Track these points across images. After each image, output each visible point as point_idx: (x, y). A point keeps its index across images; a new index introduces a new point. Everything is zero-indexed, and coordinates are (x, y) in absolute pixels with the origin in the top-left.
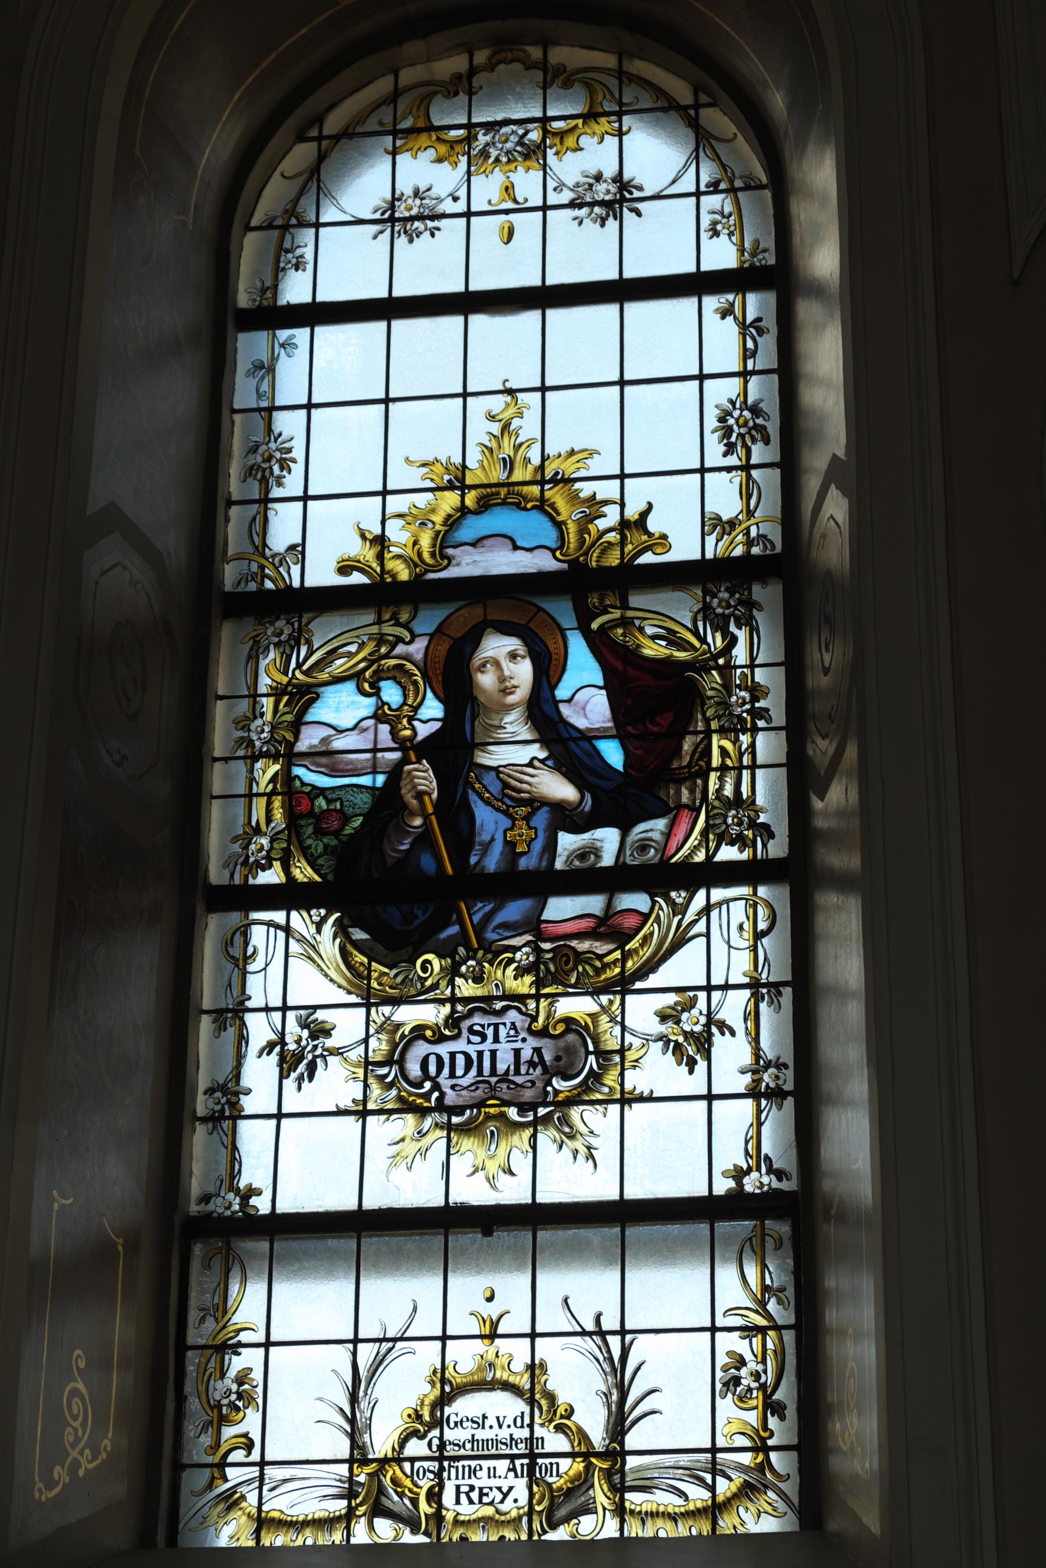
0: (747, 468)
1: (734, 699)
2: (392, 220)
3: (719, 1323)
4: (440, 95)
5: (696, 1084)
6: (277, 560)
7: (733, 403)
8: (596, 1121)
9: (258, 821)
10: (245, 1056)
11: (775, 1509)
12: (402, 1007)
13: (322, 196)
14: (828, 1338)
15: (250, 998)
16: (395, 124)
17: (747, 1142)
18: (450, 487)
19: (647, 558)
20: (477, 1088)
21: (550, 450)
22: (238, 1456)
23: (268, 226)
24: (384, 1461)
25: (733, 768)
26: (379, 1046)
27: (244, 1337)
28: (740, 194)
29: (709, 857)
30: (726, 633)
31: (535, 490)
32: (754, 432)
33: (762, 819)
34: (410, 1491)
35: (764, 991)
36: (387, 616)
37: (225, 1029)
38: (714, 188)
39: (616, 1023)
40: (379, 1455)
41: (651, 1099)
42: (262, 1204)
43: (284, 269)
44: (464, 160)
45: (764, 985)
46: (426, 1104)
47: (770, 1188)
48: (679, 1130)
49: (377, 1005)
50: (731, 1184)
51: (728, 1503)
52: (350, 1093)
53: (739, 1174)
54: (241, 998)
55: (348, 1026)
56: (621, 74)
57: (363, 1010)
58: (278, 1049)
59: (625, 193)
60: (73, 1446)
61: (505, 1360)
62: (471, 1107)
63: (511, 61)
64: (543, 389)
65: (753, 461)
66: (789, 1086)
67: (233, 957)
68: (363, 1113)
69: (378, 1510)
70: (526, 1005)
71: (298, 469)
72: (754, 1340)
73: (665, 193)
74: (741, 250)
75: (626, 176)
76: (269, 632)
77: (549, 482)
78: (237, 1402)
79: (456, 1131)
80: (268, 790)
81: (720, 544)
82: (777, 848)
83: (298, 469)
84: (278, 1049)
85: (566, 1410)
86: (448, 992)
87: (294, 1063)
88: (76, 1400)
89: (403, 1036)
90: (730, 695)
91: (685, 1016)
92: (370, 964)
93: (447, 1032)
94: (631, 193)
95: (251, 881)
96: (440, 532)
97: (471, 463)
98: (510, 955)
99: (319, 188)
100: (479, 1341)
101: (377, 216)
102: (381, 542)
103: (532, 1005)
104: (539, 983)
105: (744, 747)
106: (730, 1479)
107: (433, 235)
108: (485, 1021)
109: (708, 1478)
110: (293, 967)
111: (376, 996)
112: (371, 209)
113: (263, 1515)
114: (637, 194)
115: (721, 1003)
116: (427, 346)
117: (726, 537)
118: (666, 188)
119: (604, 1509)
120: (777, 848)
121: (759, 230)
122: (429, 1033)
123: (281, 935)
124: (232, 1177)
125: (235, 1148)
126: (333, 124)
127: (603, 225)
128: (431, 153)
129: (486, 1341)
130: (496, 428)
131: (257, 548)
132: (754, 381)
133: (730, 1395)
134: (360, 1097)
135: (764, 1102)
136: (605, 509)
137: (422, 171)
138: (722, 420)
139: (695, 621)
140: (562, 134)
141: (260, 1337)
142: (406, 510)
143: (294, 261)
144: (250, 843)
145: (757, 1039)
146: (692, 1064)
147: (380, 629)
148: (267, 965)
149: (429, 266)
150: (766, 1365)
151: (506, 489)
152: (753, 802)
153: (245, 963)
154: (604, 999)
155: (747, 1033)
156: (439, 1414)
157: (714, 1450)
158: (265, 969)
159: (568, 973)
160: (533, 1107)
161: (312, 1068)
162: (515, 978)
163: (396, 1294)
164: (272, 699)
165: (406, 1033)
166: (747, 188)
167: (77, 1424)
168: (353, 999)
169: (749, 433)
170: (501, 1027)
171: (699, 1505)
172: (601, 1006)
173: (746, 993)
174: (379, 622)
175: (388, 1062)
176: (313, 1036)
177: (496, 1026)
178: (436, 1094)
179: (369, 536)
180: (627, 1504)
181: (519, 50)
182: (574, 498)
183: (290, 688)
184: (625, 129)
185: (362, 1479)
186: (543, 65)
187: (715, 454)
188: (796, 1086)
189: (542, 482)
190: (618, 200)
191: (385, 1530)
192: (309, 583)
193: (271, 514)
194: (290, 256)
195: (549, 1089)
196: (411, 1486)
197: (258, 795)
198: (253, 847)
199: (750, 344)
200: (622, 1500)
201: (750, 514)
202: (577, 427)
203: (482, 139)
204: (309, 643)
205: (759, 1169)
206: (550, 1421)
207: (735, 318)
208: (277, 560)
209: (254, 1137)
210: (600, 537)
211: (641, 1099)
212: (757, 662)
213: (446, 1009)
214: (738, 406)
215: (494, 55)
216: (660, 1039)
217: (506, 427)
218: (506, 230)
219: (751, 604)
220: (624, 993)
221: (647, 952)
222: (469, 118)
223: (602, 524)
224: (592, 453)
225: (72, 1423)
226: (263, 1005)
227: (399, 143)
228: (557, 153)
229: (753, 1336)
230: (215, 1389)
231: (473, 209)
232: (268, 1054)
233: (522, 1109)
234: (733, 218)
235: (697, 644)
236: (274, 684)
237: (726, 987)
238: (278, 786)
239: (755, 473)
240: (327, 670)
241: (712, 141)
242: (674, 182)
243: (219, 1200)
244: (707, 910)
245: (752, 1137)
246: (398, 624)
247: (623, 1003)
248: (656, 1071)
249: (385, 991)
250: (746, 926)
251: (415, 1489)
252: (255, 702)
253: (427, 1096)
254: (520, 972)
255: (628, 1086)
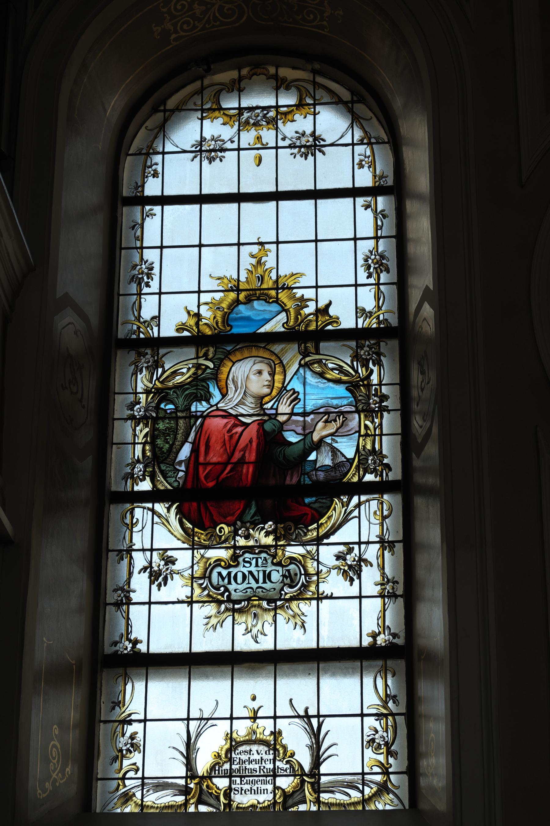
0: (378, 284)
1: (371, 401)
2: (201, 151)
3: (365, 711)
4: (224, 91)
5: (354, 590)
6: (146, 324)
7: (371, 252)
8: (307, 608)
9: (138, 456)
10: (133, 572)
11: (392, 802)
12: (210, 550)
13: (166, 139)
14: (409, 290)
15: (134, 545)
16: (202, 106)
17: (378, 619)
18: (231, 290)
19: (330, 327)
20: (247, 592)
21: (282, 273)
22: (131, 774)
23: (139, 153)
24: (203, 778)
25: (372, 435)
26: (198, 570)
27: (133, 717)
28: (374, 146)
29: (360, 479)
30: (367, 368)
31: (273, 293)
32: (381, 267)
33: (385, 461)
34: (216, 792)
35: (386, 545)
36: (201, 354)
37: (123, 560)
38: (361, 143)
39: (315, 560)
40: (200, 774)
41: (331, 597)
42: (142, 647)
43: (147, 177)
44: (237, 123)
45: (386, 542)
46: (222, 599)
47: (390, 643)
48: (348, 614)
49: (197, 549)
50: (371, 639)
51: (370, 798)
52: (184, 593)
53: (374, 636)
54: (131, 544)
55: (184, 559)
56: (315, 83)
57: (191, 551)
58: (148, 570)
59: (317, 142)
60: (54, 771)
61: (261, 730)
62: (244, 600)
63: (260, 74)
64: (278, 243)
65: (381, 282)
66: (400, 592)
67: (126, 524)
68: (190, 602)
69: (200, 801)
70: (270, 550)
71: (156, 278)
72: (382, 721)
73: (336, 143)
74: (375, 176)
75: (317, 134)
76: (143, 361)
77: (280, 289)
78: (130, 748)
79: (237, 612)
80: (143, 441)
81: (366, 322)
82: (395, 475)
83: (156, 278)
84: (148, 570)
85: (291, 754)
86: (232, 543)
87: (157, 577)
88: (54, 749)
89: (210, 564)
90: (369, 399)
91: (348, 557)
92: (193, 528)
93: (232, 563)
94: (319, 142)
95: (136, 488)
96: (227, 312)
97: (243, 278)
98: (262, 526)
99: (164, 135)
100: (249, 720)
101: (193, 149)
102: (198, 316)
103: (273, 550)
104: (276, 539)
105: (377, 424)
106: (372, 788)
107: (221, 160)
108: (251, 556)
109: (361, 787)
110: (155, 530)
111: (198, 545)
112: (190, 145)
113: (144, 803)
114: (322, 143)
115: (366, 550)
116: (220, 216)
117: (368, 319)
118: (338, 140)
119: (310, 801)
120: (395, 475)
121: (384, 164)
122: (223, 564)
123: (150, 513)
124: (128, 634)
125: (128, 619)
126: (171, 103)
127: (306, 159)
128: (221, 120)
129: (252, 720)
130: (254, 261)
131: (136, 318)
132: (381, 241)
133: (371, 748)
134: (189, 595)
135: (386, 600)
136: (308, 303)
137: (214, 128)
138: (366, 260)
139: (352, 362)
140: (285, 114)
141: (142, 717)
142: (209, 301)
143: (152, 172)
144: (134, 468)
145: (383, 568)
146: (352, 580)
147: (198, 361)
148: (143, 528)
149: (219, 177)
150: (388, 733)
151: (259, 292)
152: (381, 452)
153: (132, 528)
154: (309, 548)
155: (378, 565)
156: (229, 756)
157: (363, 774)
158: (142, 530)
159: (292, 534)
160: (275, 601)
161: (165, 580)
162: (265, 536)
163: (210, 692)
164: (145, 395)
165: (212, 563)
166: (377, 143)
167: (55, 761)
168: (186, 546)
169: (379, 267)
170: (259, 559)
171: (356, 800)
172: (307, 551)
173: (378, 546)
174: (197, 358)
175: (203, 577)
176: (166, 564)
177: (257, 559)
178: (227, 593)
179: (192, 313)
180: (321, 799)
181: (264, 68)
182: (293, 297)
183: (153, 390)
184: (317, 112)
185: (192, 786)
186: (276, 77)
187: (362, 278)
188: (405, 591)
189: (277, 289)
190: (312, 146)
191: (203, 809)
192: (162, 335)
193: (142, 300)
194: (150, 169)
195: (283, 592)
196: (216, 789)
197: (138, 443)
198: (136, 469)
199: (379, 223)
200: (319, 797)
201: (379, 308)
202: (293, 262)
203: (246, 115)
204: (163, 367)
205: (384, 634)
206: (284, 758)
207: (372, 209)
208: (146, 324)
209: (137, 613)
210: (306, 318)
211: (327, 597)
212: (383, 383)
213: (231, 552)
214: (373, 253)
215: (251, 70)
216: (336, 568)
217: (259, 262)
218: (258, 158)
219: (379, 354)
220: (318, 545)
221: (330, 524)
222: (240, 105)
223: (307, 311)
224: (302, 275)
225: (53, 761)
226: (141, 548)
227: (204, 115)
228: (283, 122)
229: (381, 719)
230: (120, 742)
231: (241, 147)
232: (144, 572)
233: (269, 601)
234: (370, 158)
235: (354, 373)
236: (146, 388)
237: (368, 543)
238: (148, 439)
239: (381, 287)
240: (172, 382)
241: (361, 121)
242: (341, 138)
243: (121, 645)
244: (358, 505)
245: (381, 617)
246: (207, 359)
247: (318, 550)
248: (334, 584)
249: (200, 542)
250: (378, 513)
251: (218, 791)
252: (136, 396)
253: (222, 595)
254: (267, 534)
255: (321, 591)
